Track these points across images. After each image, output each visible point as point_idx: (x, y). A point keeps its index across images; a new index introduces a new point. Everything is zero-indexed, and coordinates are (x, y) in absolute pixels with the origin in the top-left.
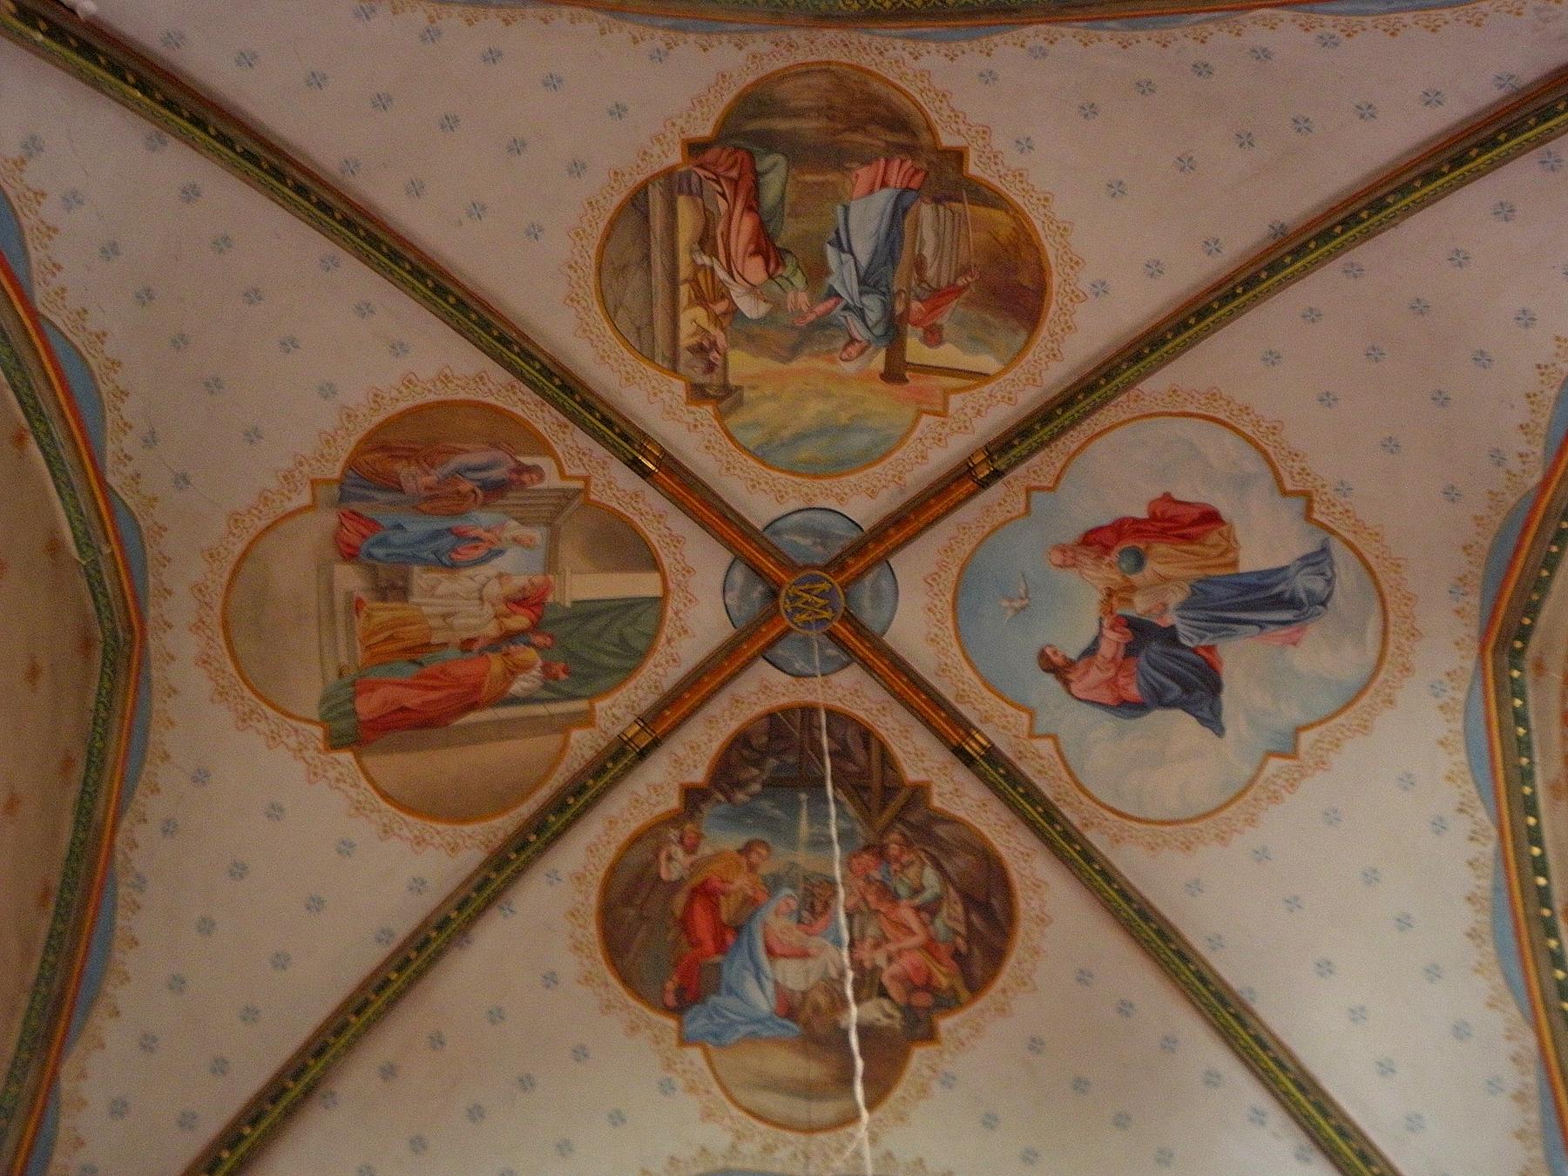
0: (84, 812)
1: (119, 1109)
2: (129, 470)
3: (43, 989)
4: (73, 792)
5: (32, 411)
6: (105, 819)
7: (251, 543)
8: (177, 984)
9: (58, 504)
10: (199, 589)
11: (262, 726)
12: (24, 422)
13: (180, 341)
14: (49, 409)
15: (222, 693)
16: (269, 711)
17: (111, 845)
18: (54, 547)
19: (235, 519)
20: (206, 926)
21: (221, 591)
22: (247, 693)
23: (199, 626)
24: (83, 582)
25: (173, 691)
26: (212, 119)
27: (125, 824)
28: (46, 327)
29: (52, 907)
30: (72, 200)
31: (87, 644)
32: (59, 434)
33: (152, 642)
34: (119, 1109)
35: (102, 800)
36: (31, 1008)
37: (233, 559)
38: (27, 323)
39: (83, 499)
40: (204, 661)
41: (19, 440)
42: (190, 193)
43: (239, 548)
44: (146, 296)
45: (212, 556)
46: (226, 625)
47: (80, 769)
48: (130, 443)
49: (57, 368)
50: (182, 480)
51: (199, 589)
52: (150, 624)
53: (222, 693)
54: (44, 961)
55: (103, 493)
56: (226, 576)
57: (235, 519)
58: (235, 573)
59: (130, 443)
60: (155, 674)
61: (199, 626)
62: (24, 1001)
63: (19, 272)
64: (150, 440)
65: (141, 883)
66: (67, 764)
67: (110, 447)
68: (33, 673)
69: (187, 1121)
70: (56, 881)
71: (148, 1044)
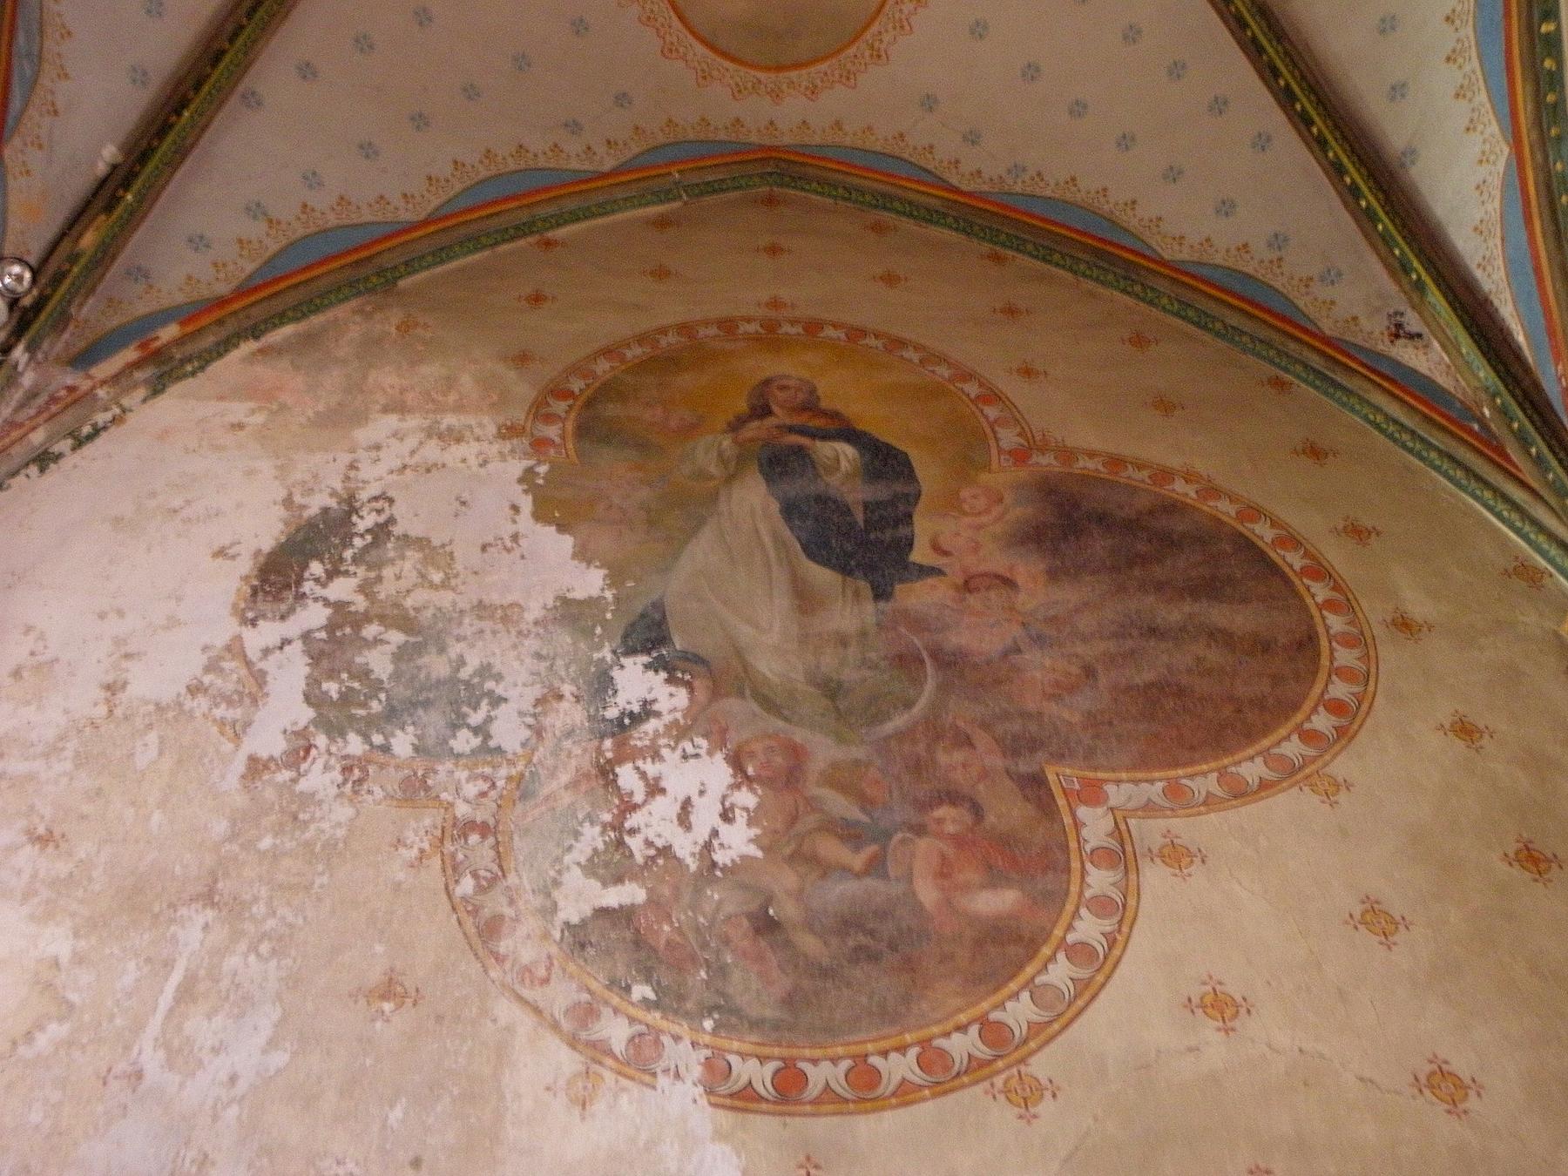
0: (930, 216)
1: (1226, 208)
2: (601, 150)
3: (1082, 267)
4: (907, 224)
5: (521, 231)
6: (942, 198)
7: (693, 33)
8: (1125, 142)
9: (619, 217)
10: (738, 92)
11: (887, 38)
12: (530, 239)
13: (471, 92)
14: (524, 216)
15: (848, 77)
16: (875, 28)
17: (970, 195)
18: (662, 223)
19: (668, 51)
20: (1078, 109)
21: (743, 70)
22: (851, 51)
23: (776, 95)
24: (709, 199)
25: (838, 125)
26: (216, 46)
27: (954, 181)
28: (443, 212)
29: (1010, 253)
30: (312, 179)
31: (770, 201)
32: (551, 210)
33: (787, 140)
34: (1226, 208)
35: (923, 199)
36: (1097, 280)
37: (711, 55)
38: (432, 229)
39: (619, 194)
40: (813, 92)
41: (548, 244)
42: (307, 71)
43: (700, 49)
44: (420, 121)
45: (705, 76)
46: (779, 68)
47: (887, 217)
48: (573, 146)
49: (480, 208)
50: (622, 99)
51: (738, 92)
52: (767, 141)
53: (848, 77)
54: (1057, 265)
55: (622, 174)
56: (727, 64)
57: (668, 51)
58: (725, 55)
59: (573, 146)
60: (817, 140)
61: (776, 95)
62: (1090, 285)
63: (388, 229)
64: (574, 127)
65: (1018, 169)
66: (878, 228)
67: (574, 165)
68: (774, 250)
69: (1262, 142)
70: (986, 247)
71: (1173, 174)
